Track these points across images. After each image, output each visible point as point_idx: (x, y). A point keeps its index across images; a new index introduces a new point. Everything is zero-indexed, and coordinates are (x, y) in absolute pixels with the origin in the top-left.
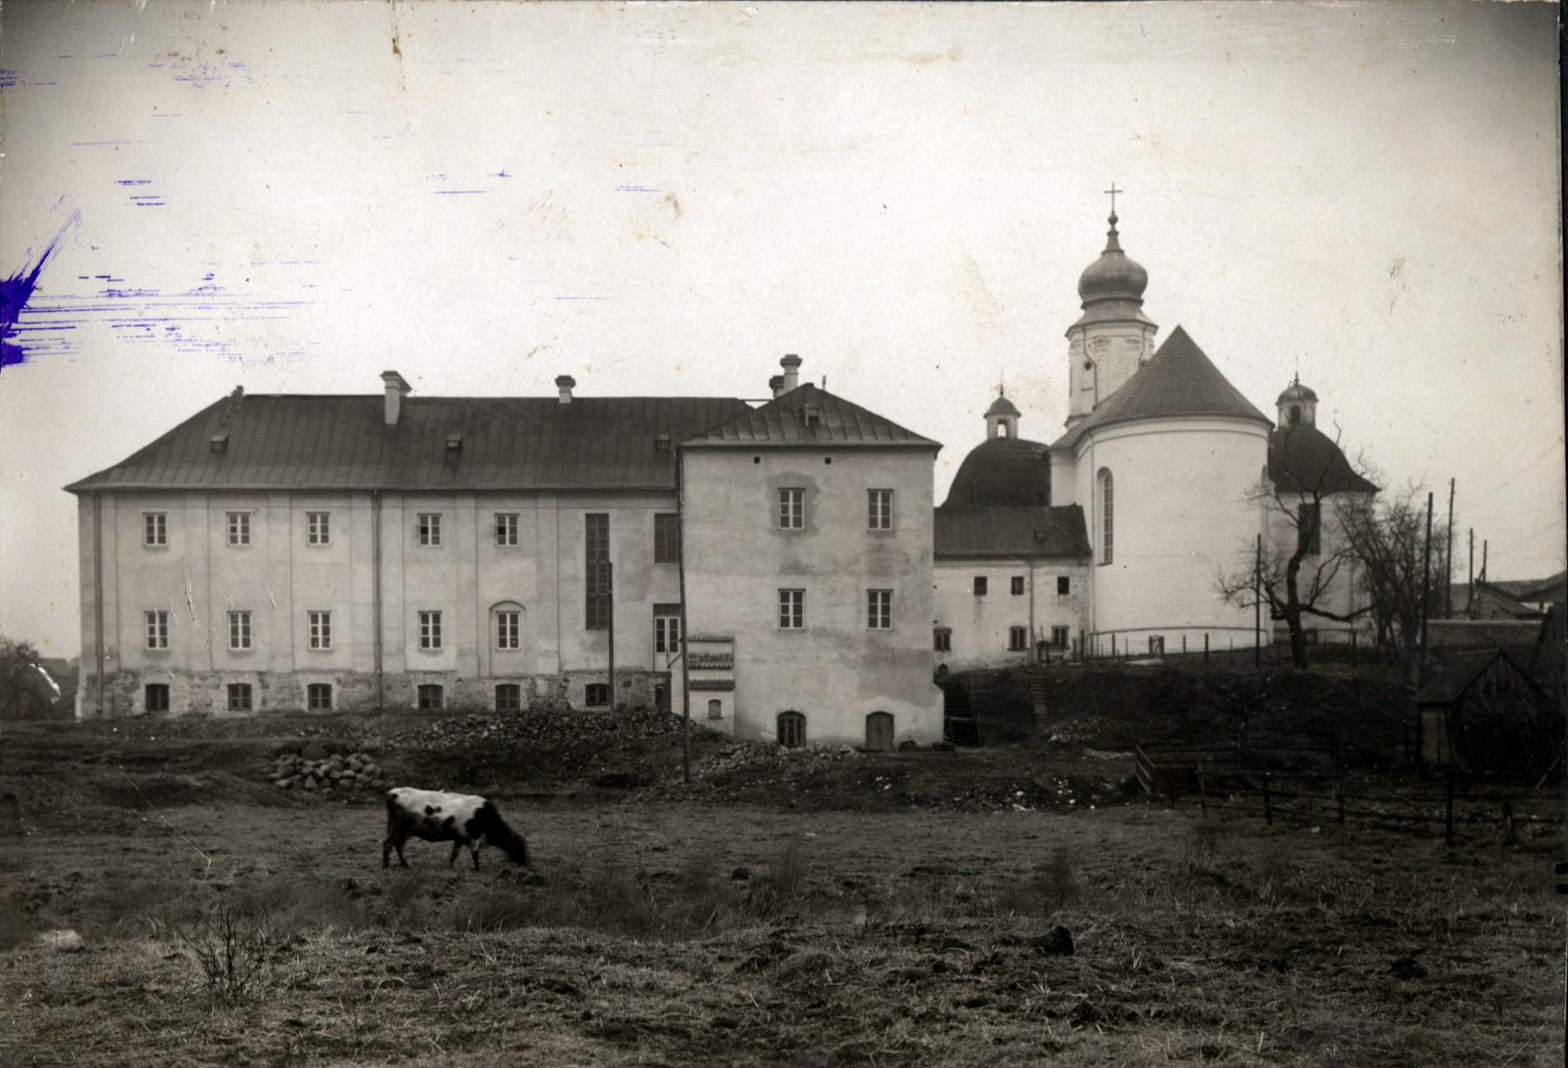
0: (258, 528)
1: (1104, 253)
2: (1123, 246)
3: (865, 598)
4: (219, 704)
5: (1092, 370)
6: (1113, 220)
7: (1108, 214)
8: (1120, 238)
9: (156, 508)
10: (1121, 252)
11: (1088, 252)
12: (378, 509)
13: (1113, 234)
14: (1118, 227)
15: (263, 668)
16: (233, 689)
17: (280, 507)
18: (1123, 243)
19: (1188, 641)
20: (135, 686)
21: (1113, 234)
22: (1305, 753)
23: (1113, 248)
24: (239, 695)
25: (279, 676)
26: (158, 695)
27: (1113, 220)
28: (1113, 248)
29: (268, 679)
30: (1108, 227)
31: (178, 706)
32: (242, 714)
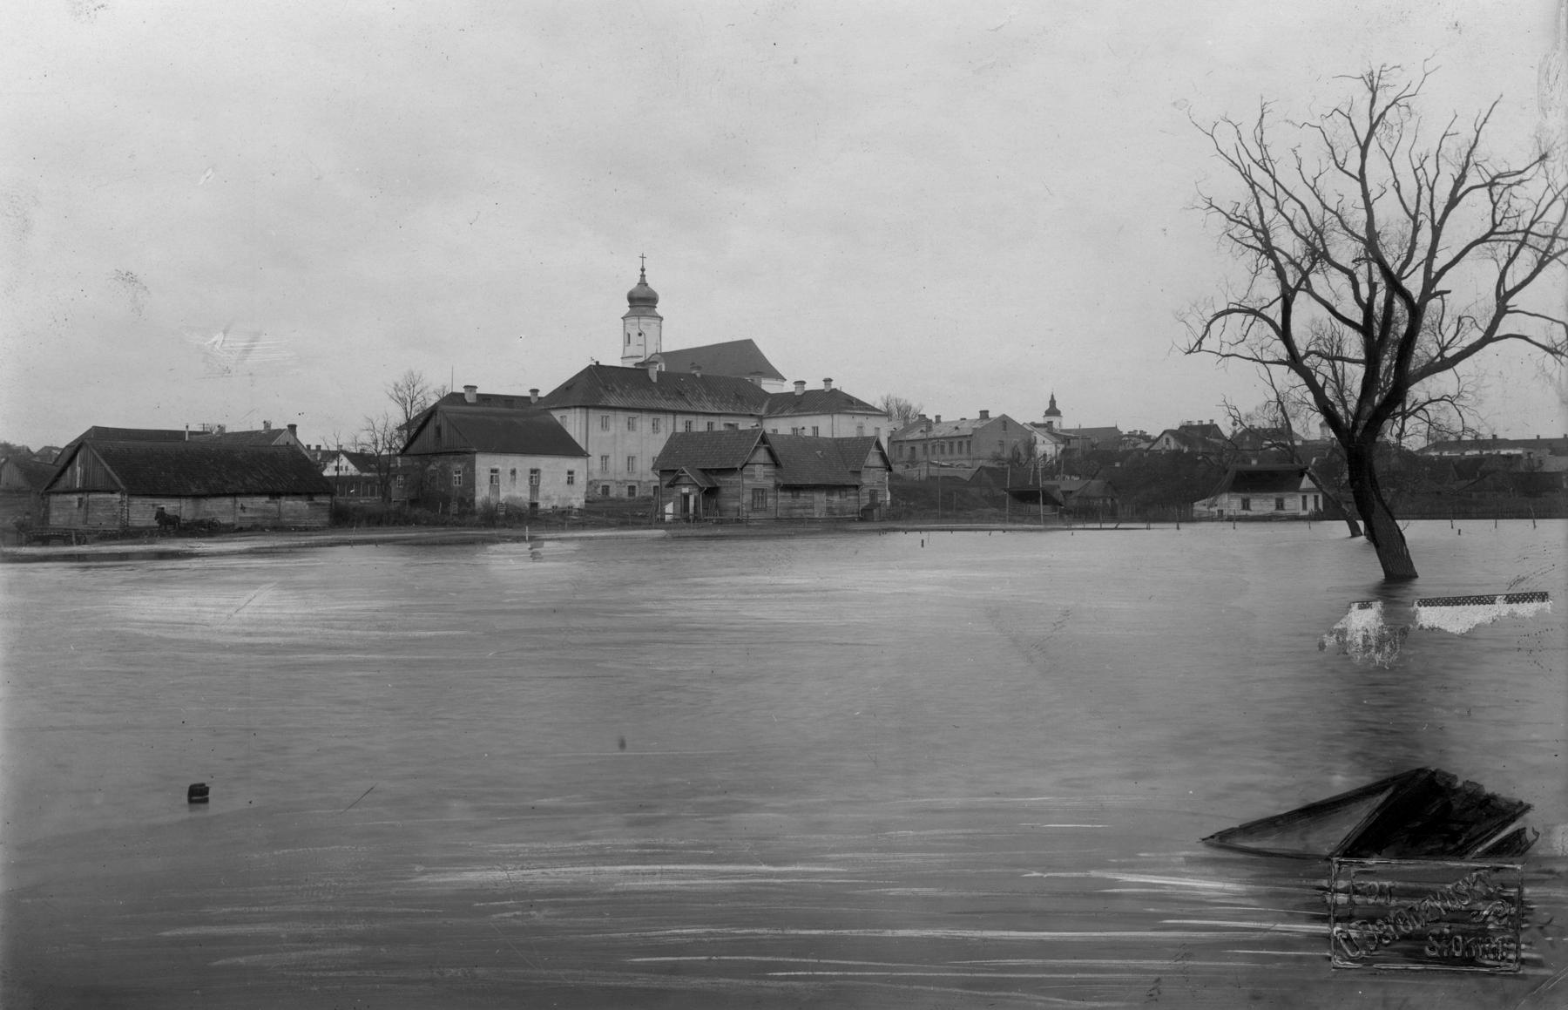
0: (638, 424)
1: (639, 284)
2: (647, 281)
3: (626, 461)
4: (625, 492)
5: (643, 336)
6: (643, 270)
7: (641, 267)
8: (646, 278)
9: (658, 416)
10: (646, 285)
11: (632, 283)
12: (675, 415)
13: (643, 276)
14: (645, 273)
15: (639, 479)
16: (630, 487)
17: (645, 416)
18: (648, 280)
19: (1494, 525)
20: (598, 486)
21: (643, 276)
22: (332, 622)
23: (643, 283)
24: (632, 488)
25: (645, 483)
26: (606, 489)
27: (643, 270)
28: (643, 283)
29: (642, 484)
30: (641, 273)
31: (613, 494)
32: (631, 498)
